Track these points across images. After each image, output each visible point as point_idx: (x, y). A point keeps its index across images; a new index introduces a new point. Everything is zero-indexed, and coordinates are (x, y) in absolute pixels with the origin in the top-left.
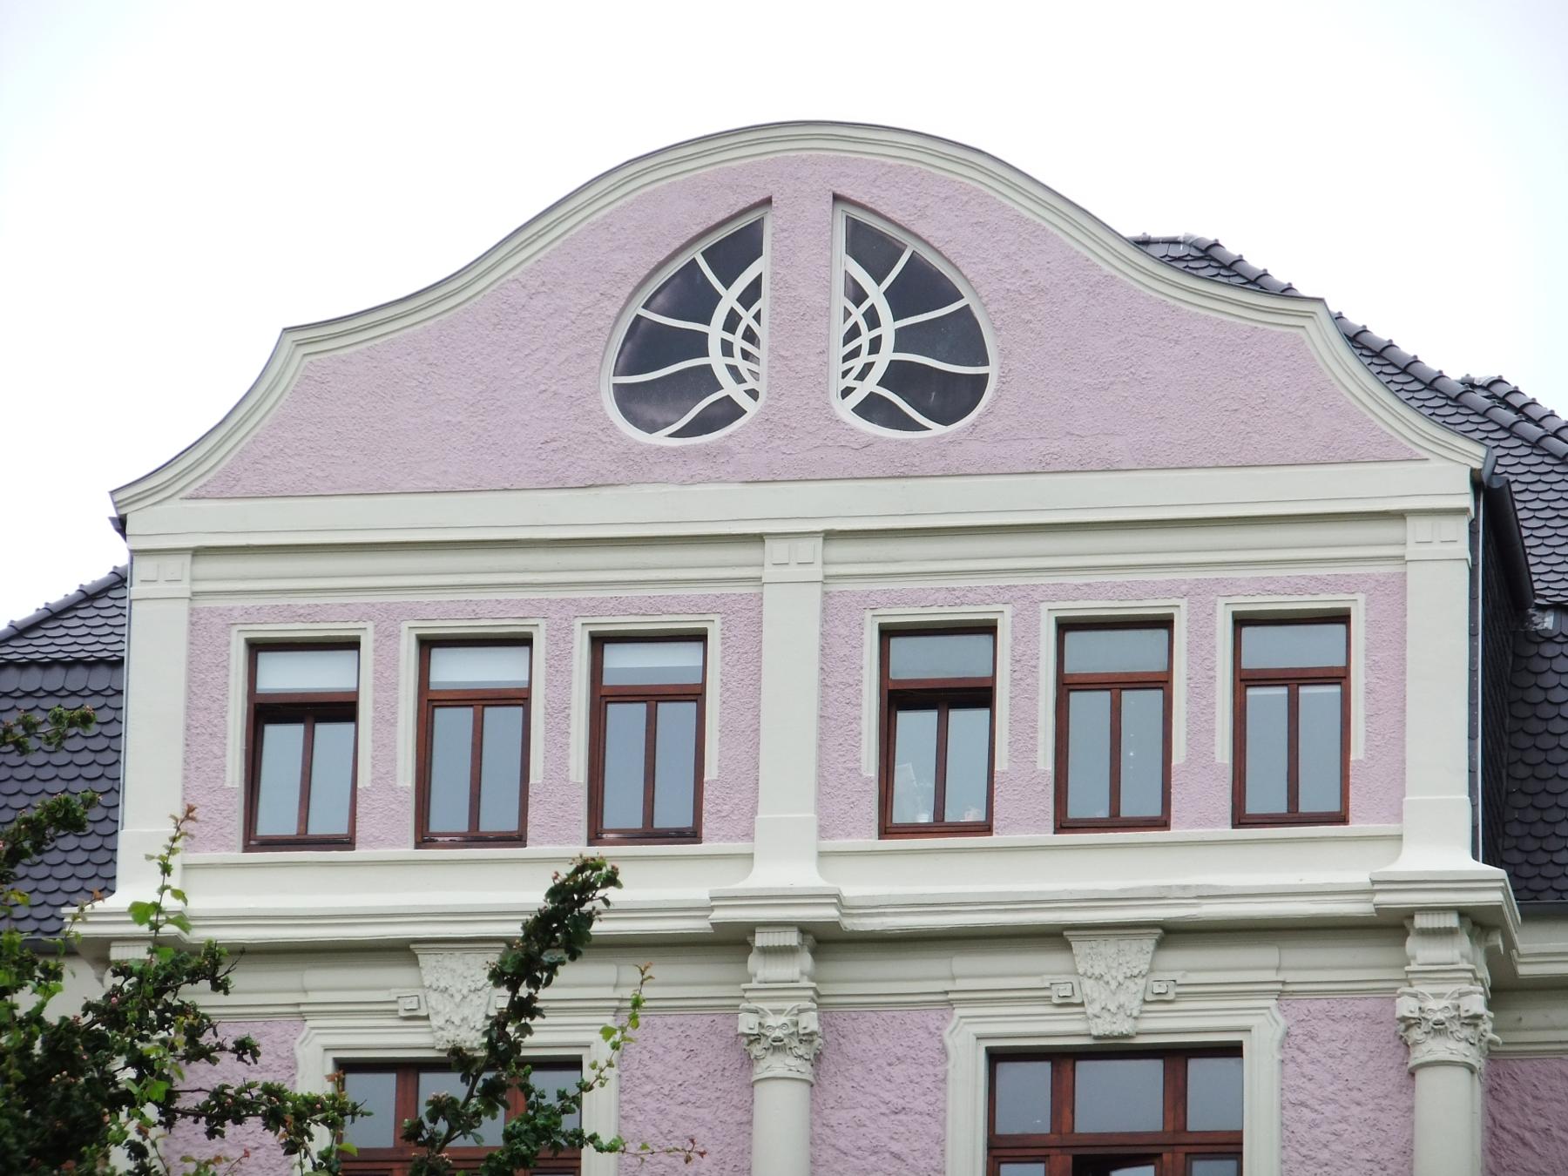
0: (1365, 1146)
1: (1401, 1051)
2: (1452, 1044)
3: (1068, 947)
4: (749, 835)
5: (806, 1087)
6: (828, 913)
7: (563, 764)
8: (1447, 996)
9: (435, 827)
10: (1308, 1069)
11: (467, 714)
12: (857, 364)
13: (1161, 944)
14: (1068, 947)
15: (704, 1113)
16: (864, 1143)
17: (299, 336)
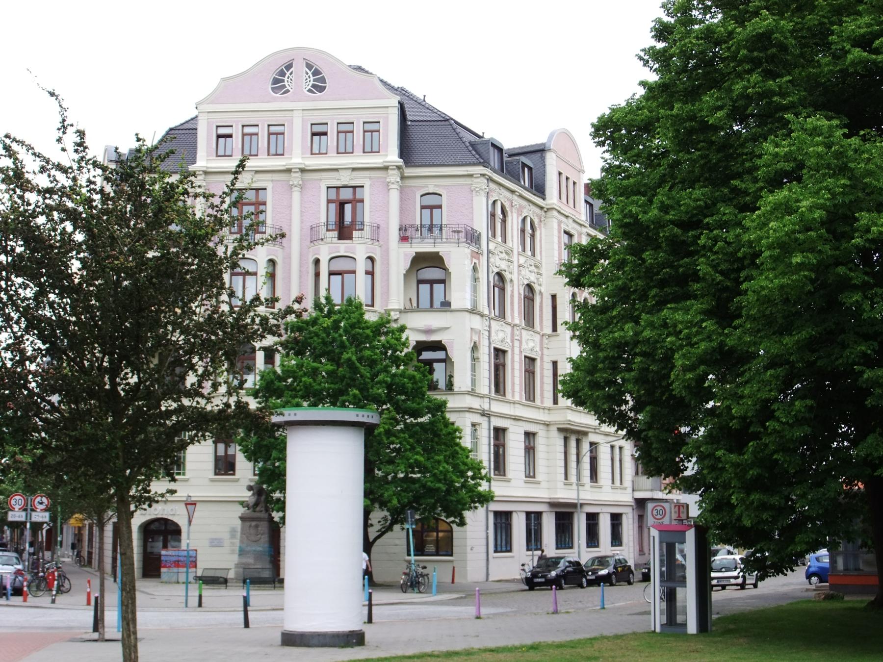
6: (303, 166)
11: (344, 134)
17: (224, 80)
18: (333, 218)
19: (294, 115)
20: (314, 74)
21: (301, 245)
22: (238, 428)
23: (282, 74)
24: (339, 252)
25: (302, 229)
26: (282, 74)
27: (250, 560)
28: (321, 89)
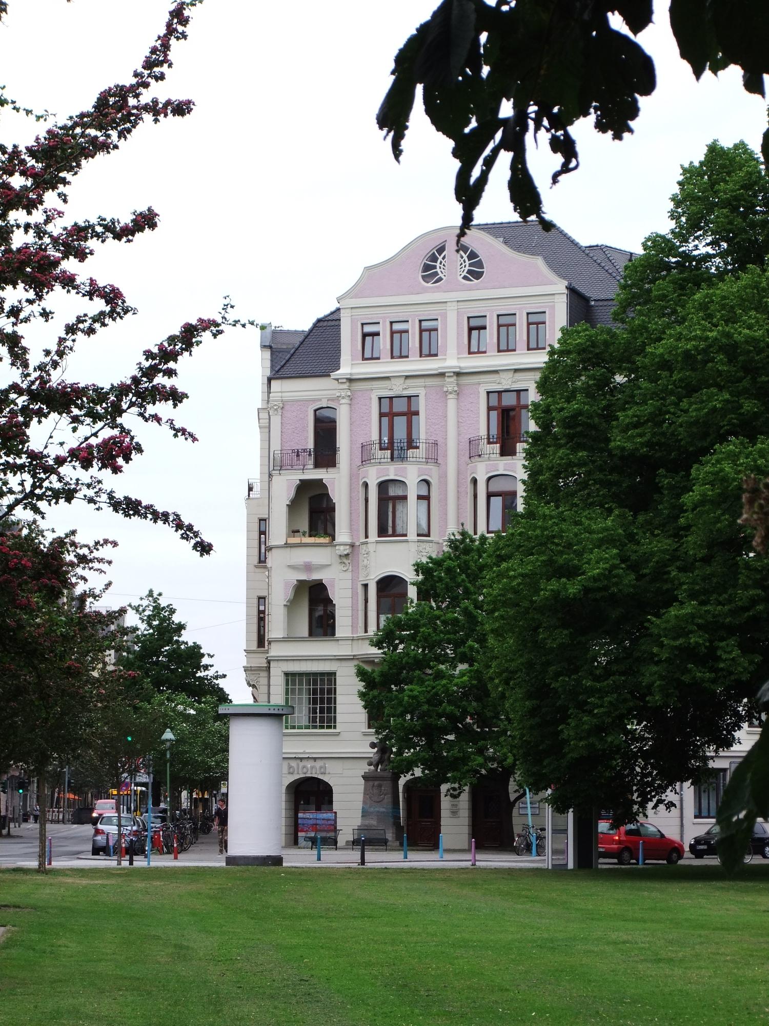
6: (457, 370)
11: (399, 334)
12: (462, 270)
17: (367, 269)
19: (448, 308)
20: (470, 258)
22: (98, 680)
23: (434, 258)
24: (498, 470)
26: (434, 258)
27: (374, 822)
28: (478, 275)
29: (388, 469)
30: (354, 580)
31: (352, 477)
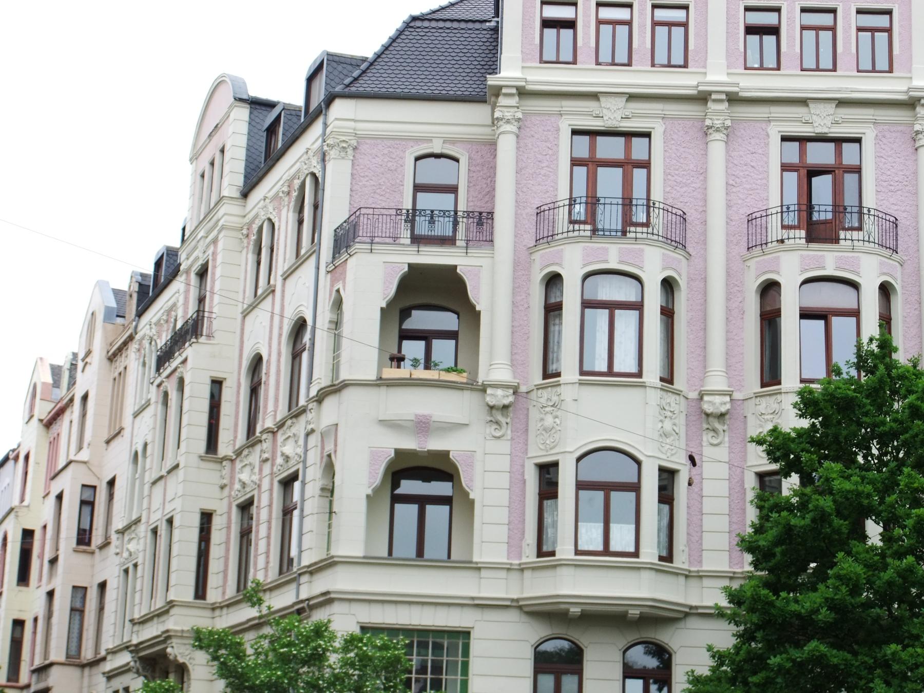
0: (902, 170)
1: (913, 142)
2: (512, 126)
3: (807, 105)
4: (705, 67)
5: (724, 143)
6: (523, 84)
7: (644, 42)
8: (323, 106)
9: (656, 62)
10: (883, 146)
13: (837, 106)
14: (807, 105)
15: (690, 151)
16: (742, 162)
18: (792, 198)
21: (728, 253)
25: (729, 220)
29: (606, 250)
30: (518, 459)
31: (520, 267)
